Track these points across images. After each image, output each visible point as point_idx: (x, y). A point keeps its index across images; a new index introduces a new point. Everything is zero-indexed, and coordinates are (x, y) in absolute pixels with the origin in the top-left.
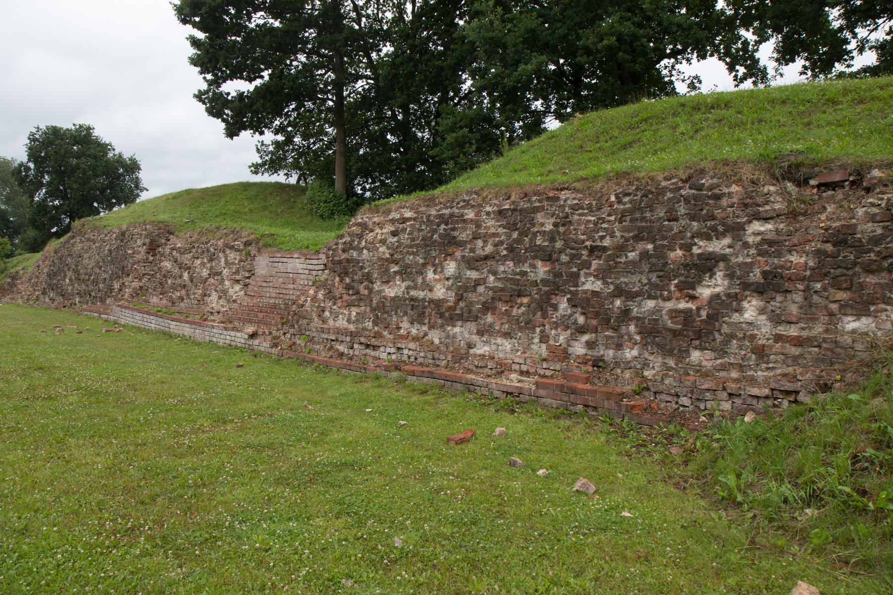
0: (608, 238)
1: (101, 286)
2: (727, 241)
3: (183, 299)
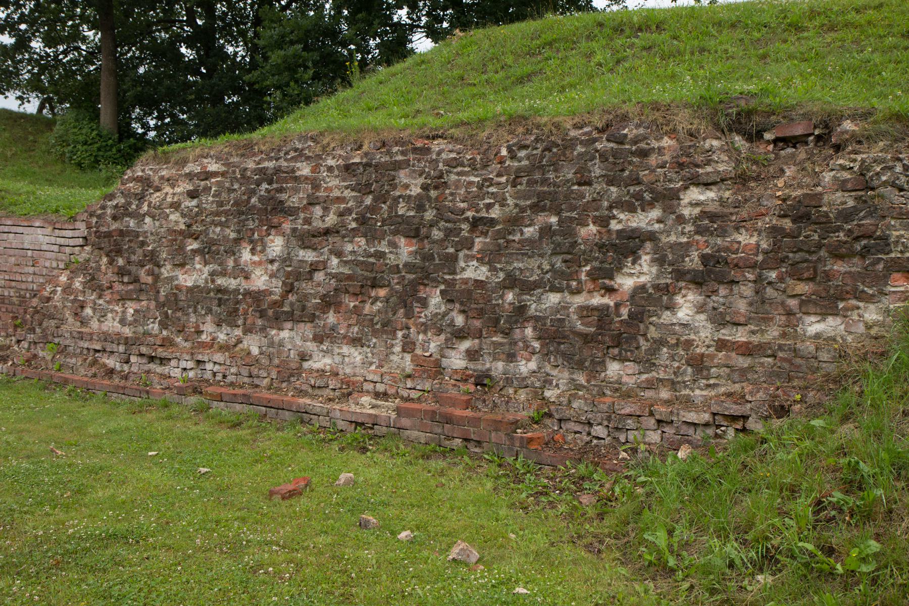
0: (497, 206)
2: (655, 213)
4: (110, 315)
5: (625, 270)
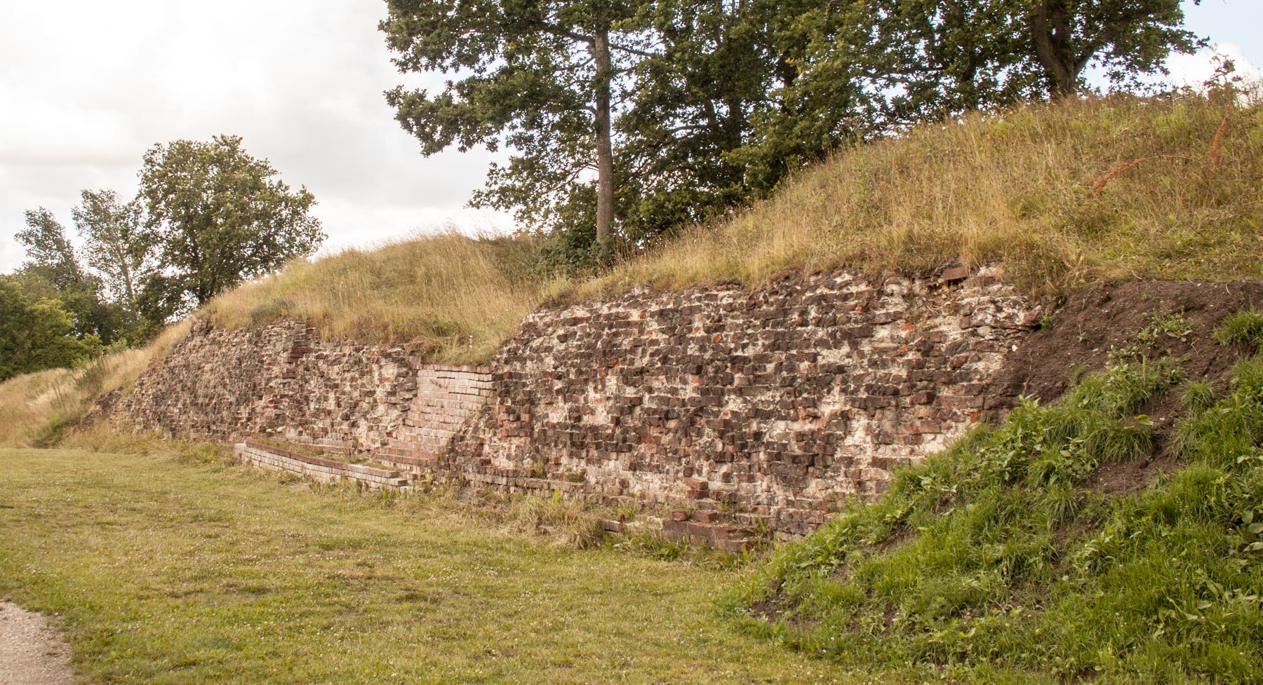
0: (750, 346)
1: (225, 413)
2: (846, 349)
3: (327, 433)
4: (501, 451)
5: (824, 400)
